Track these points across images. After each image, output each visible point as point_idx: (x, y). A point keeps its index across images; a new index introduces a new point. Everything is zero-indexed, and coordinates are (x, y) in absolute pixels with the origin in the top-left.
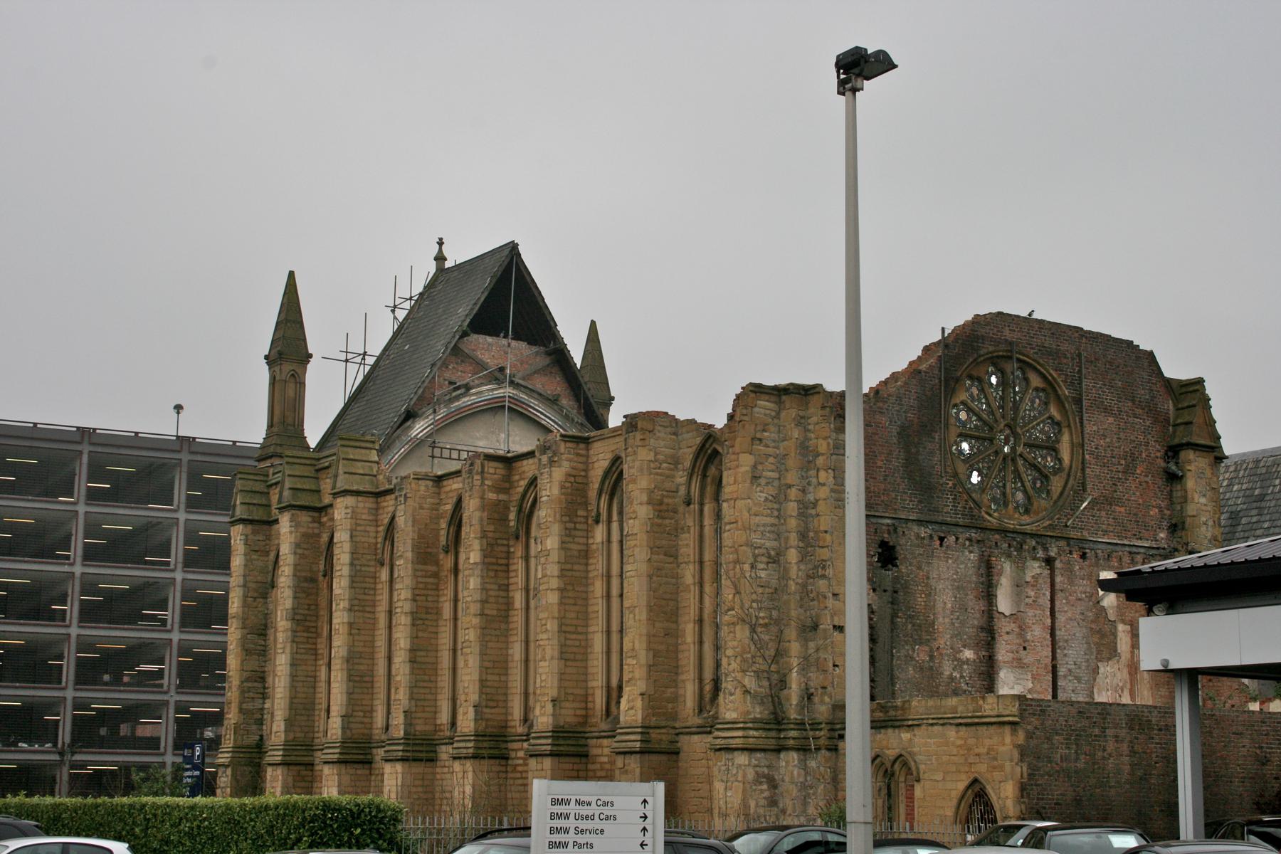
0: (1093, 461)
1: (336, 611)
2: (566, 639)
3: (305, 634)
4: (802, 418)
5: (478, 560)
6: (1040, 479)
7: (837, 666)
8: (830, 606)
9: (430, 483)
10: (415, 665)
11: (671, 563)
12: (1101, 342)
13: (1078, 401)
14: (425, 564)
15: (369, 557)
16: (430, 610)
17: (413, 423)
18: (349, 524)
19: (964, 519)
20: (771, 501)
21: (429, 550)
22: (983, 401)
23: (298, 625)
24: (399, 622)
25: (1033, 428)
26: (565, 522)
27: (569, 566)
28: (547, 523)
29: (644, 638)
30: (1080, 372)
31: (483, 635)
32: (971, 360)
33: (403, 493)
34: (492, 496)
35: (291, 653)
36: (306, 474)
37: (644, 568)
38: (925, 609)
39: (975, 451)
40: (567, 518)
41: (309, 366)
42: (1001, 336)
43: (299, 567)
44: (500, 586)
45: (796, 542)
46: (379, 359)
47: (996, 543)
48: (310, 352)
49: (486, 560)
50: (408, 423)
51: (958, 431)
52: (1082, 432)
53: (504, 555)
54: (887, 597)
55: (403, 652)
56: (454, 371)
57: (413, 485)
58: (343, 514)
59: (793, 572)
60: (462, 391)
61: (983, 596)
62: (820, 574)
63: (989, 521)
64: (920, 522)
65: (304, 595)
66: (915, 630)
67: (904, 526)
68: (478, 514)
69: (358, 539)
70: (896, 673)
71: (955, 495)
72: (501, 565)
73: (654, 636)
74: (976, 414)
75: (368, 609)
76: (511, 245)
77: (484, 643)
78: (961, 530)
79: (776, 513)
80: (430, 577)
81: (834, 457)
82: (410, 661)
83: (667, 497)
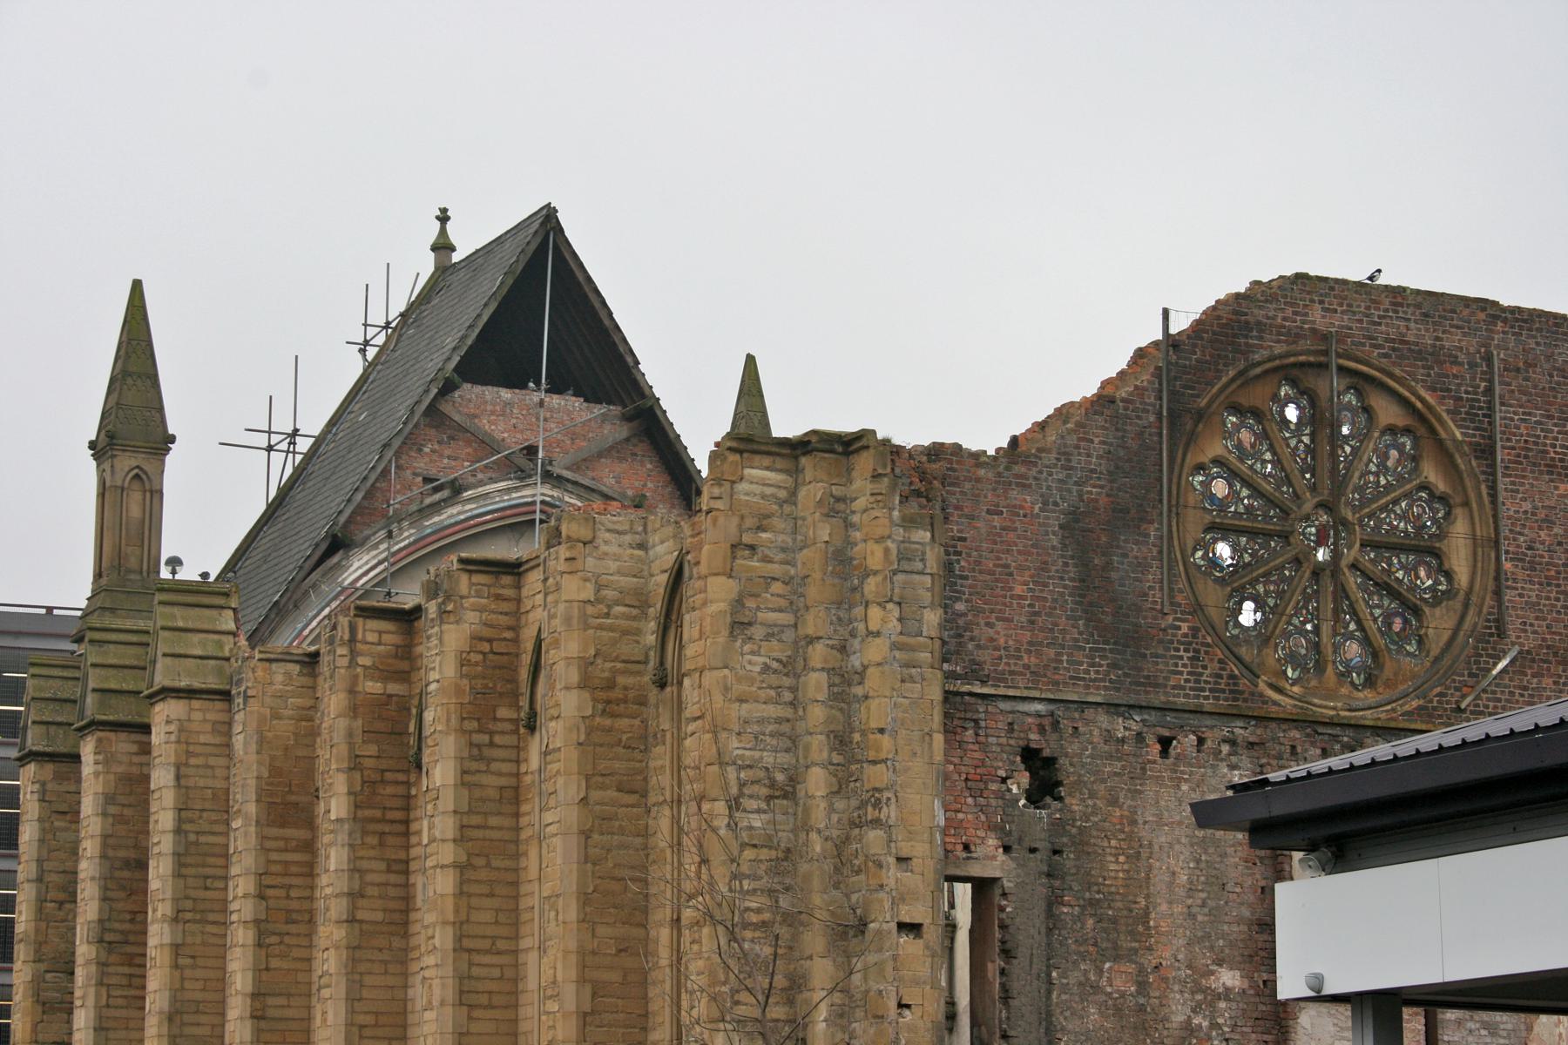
0: (1521, 574)
1: (153, 922)
2: (471, 964)
3: (126, 970)
4: (838, 500)
5: (343, 814)
6: (1402, 615)
7: (908, 1006)
8: (892, 883)
9: (296, 668)
10: (263, 1024)
11: (633, 806)
12: (1539, 330)
13: (1485, 452)
14: (282, 826)
15: (214, 816)
16: (294, 916)
17: (347, 557)
18: (173, 753)
19: (1215, 698)
20: (775, 671)
21: (293, 798)
22: (1268, 456)
23: (110, 952)
24: (235, 941)
25: (1384, 508)
26: (471, 732)
27: (475, 820)
28: (436, 735)
29: (573, 958)
30: (1489, 391)
31: (354, 961)
32: (1232, 373)
33: (242, 689)
34: (373, 687)
35: (95, 1007)
36: (127, 663)
37: (572, 816)
38: (1127, 886)
39: (1247, 558)
40: (475, 724)
41: (168, 458)
42: (1304, 322)
43: (111, 841)
44: (390, 862)
45: (825, 755)
46: (319, 441)
47: (1293, 747)
48: (171, 431)
49: (360, 813)
50: (335, 559)
51: (1208, 518)
52: (1495, 516)
53: (399, 803)
54: (1038, 863)
55: (240, 997)
56: (435, 457)
57: (260, 673)
58: (162, 735)
59: (819, 816)
60: (445, 493)
61: (1261, 859)
62: (869, 818)
63: (1275, 703)
64: (1112, 708)
65: (122, 895)
66: (1105, 930)
67: (1077, 715)
68: (342, 724)
69: (191, 783)
70: (1059, 1020)
71: (1196, 651)
72: (393, 822)
73: (594, 953)
74: (1246, 483)
75: (211, 917)
76: (544, 212)
77: (357, 977)
78: (1209, 721)
79: (788, 696)
80: (294, 851)
81: (900, 577)
82: (253, 1017)
83: (624, 672)
